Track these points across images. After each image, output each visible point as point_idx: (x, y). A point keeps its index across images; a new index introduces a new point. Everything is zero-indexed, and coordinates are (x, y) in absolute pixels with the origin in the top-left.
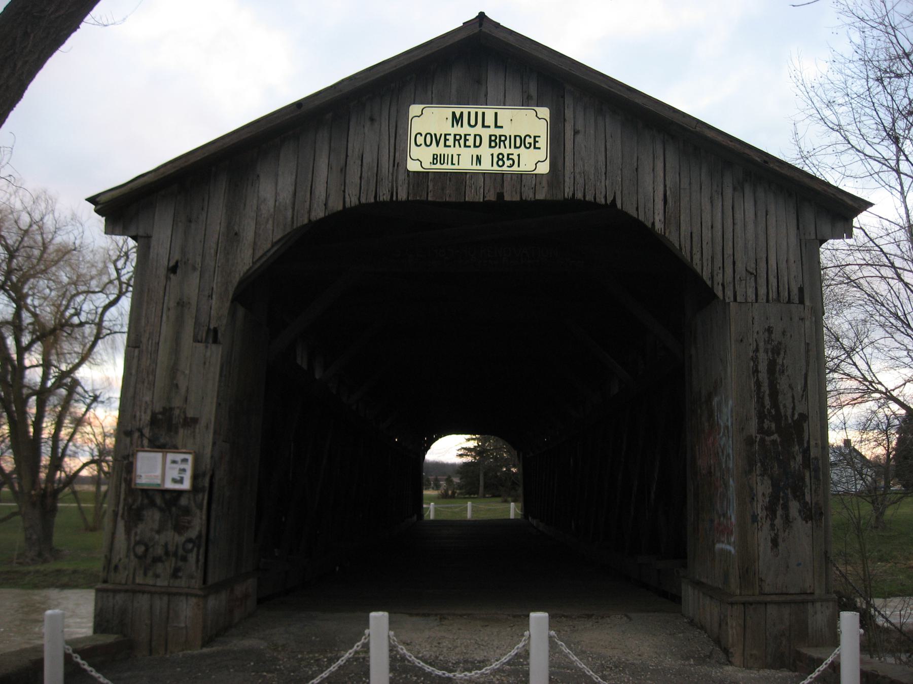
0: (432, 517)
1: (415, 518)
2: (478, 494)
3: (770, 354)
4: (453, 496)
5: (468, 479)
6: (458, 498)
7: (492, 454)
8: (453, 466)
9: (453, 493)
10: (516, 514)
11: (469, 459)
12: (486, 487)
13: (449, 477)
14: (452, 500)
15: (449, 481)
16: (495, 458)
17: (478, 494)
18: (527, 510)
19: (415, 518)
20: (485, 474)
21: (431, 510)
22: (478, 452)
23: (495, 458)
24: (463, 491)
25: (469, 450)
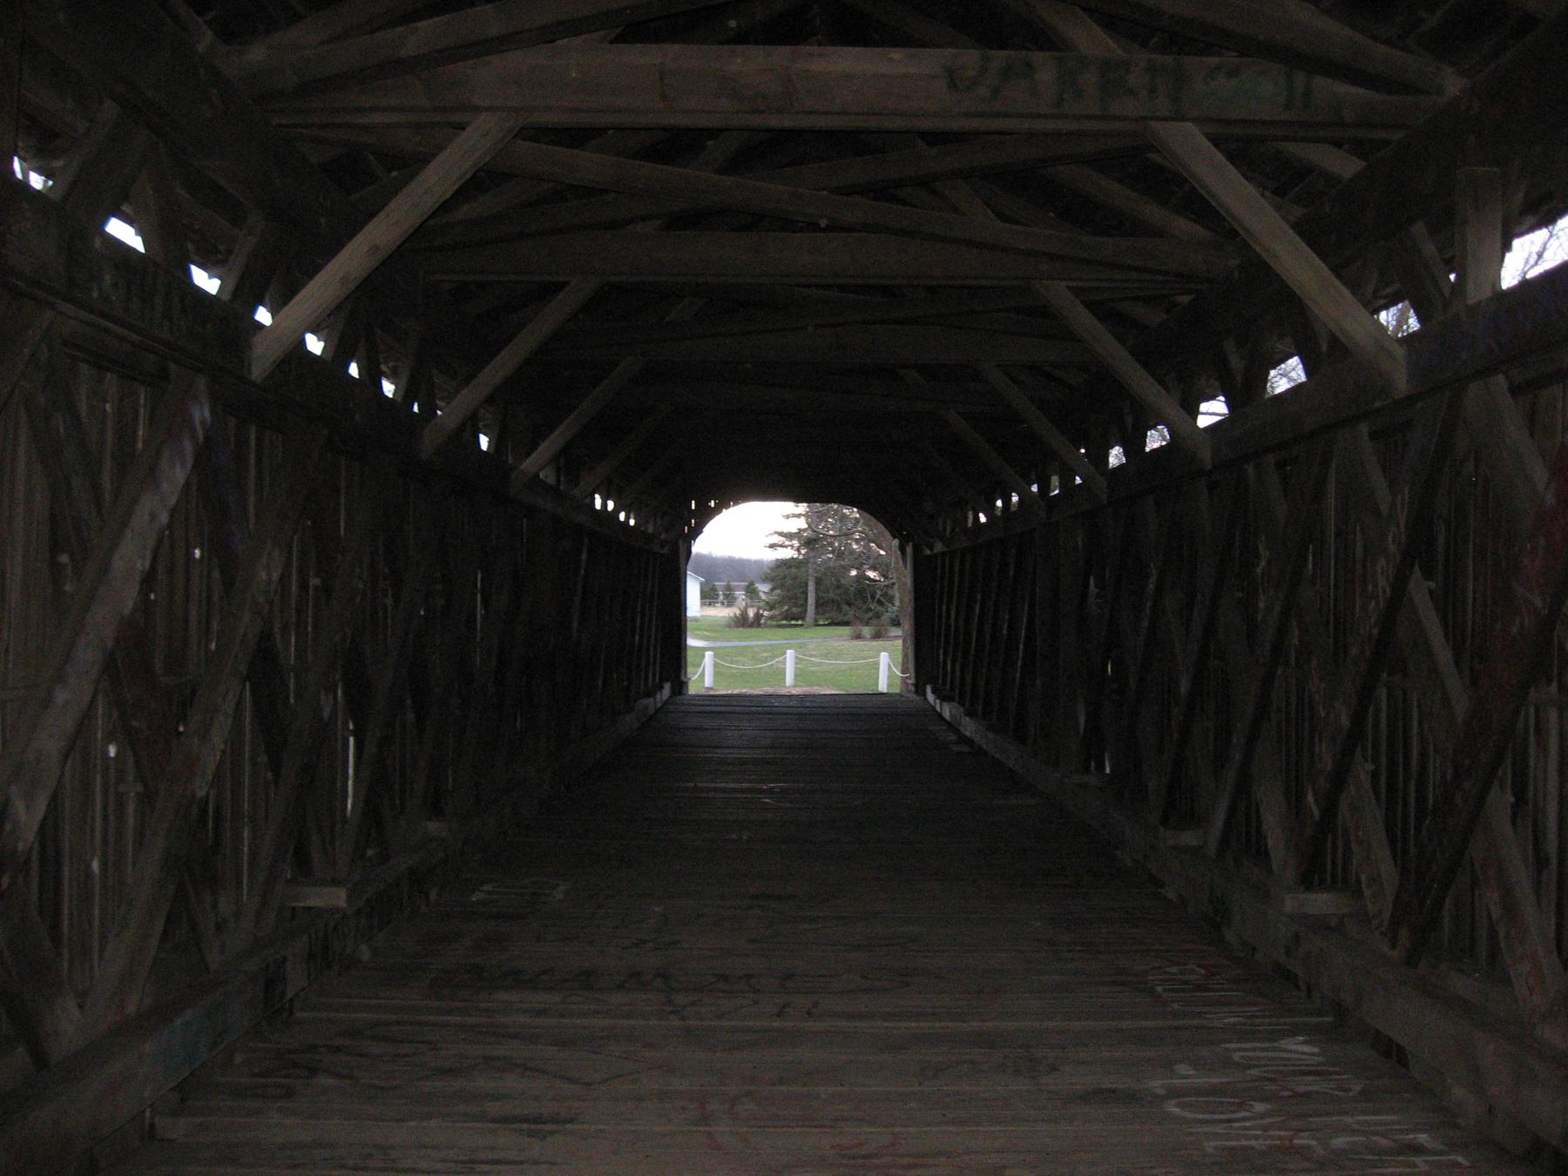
0: (708, 681)
1: (667, 691)
2: (803, 618)
3: (215, 738)
4: (757, 622)
5: (800, 595)
6: (766, 626)
7: (831, 544)
8: (758, 563)
9: (758, 616)
10: (891, 676)
11: (787, 554)
12: (820, 604)
13: (752, 584)
14: (753, 631)
15: (751, 591)
16: (840, 555)
17: (803, 618)
18: (924, 661)
19: (667, 691)
20: (818, 582)
21: (706, 673)
22: (811, 542)
23: (840, 555)
24: (776, 612)
25: (789, 536)
